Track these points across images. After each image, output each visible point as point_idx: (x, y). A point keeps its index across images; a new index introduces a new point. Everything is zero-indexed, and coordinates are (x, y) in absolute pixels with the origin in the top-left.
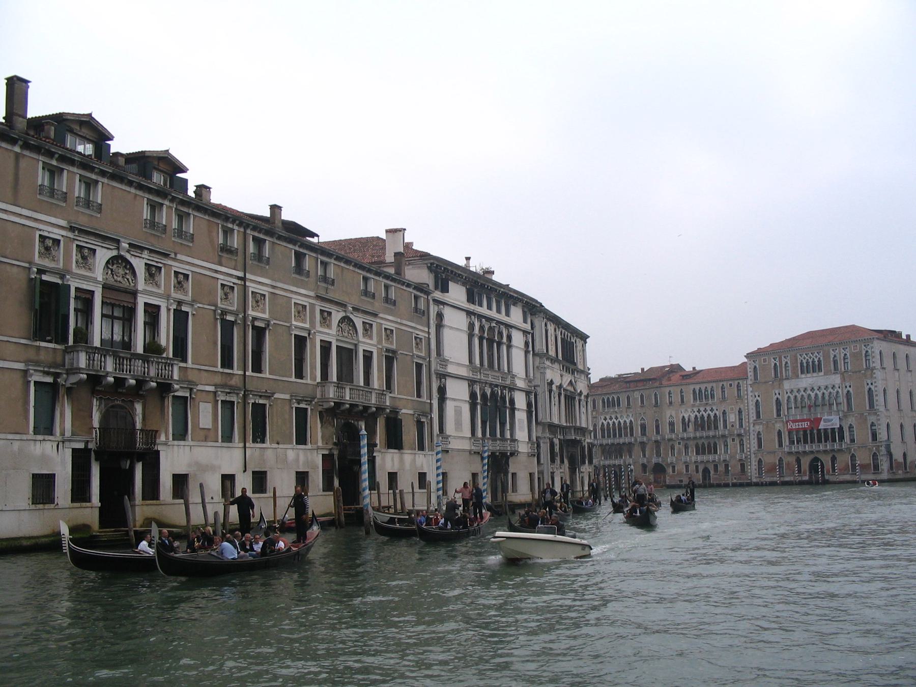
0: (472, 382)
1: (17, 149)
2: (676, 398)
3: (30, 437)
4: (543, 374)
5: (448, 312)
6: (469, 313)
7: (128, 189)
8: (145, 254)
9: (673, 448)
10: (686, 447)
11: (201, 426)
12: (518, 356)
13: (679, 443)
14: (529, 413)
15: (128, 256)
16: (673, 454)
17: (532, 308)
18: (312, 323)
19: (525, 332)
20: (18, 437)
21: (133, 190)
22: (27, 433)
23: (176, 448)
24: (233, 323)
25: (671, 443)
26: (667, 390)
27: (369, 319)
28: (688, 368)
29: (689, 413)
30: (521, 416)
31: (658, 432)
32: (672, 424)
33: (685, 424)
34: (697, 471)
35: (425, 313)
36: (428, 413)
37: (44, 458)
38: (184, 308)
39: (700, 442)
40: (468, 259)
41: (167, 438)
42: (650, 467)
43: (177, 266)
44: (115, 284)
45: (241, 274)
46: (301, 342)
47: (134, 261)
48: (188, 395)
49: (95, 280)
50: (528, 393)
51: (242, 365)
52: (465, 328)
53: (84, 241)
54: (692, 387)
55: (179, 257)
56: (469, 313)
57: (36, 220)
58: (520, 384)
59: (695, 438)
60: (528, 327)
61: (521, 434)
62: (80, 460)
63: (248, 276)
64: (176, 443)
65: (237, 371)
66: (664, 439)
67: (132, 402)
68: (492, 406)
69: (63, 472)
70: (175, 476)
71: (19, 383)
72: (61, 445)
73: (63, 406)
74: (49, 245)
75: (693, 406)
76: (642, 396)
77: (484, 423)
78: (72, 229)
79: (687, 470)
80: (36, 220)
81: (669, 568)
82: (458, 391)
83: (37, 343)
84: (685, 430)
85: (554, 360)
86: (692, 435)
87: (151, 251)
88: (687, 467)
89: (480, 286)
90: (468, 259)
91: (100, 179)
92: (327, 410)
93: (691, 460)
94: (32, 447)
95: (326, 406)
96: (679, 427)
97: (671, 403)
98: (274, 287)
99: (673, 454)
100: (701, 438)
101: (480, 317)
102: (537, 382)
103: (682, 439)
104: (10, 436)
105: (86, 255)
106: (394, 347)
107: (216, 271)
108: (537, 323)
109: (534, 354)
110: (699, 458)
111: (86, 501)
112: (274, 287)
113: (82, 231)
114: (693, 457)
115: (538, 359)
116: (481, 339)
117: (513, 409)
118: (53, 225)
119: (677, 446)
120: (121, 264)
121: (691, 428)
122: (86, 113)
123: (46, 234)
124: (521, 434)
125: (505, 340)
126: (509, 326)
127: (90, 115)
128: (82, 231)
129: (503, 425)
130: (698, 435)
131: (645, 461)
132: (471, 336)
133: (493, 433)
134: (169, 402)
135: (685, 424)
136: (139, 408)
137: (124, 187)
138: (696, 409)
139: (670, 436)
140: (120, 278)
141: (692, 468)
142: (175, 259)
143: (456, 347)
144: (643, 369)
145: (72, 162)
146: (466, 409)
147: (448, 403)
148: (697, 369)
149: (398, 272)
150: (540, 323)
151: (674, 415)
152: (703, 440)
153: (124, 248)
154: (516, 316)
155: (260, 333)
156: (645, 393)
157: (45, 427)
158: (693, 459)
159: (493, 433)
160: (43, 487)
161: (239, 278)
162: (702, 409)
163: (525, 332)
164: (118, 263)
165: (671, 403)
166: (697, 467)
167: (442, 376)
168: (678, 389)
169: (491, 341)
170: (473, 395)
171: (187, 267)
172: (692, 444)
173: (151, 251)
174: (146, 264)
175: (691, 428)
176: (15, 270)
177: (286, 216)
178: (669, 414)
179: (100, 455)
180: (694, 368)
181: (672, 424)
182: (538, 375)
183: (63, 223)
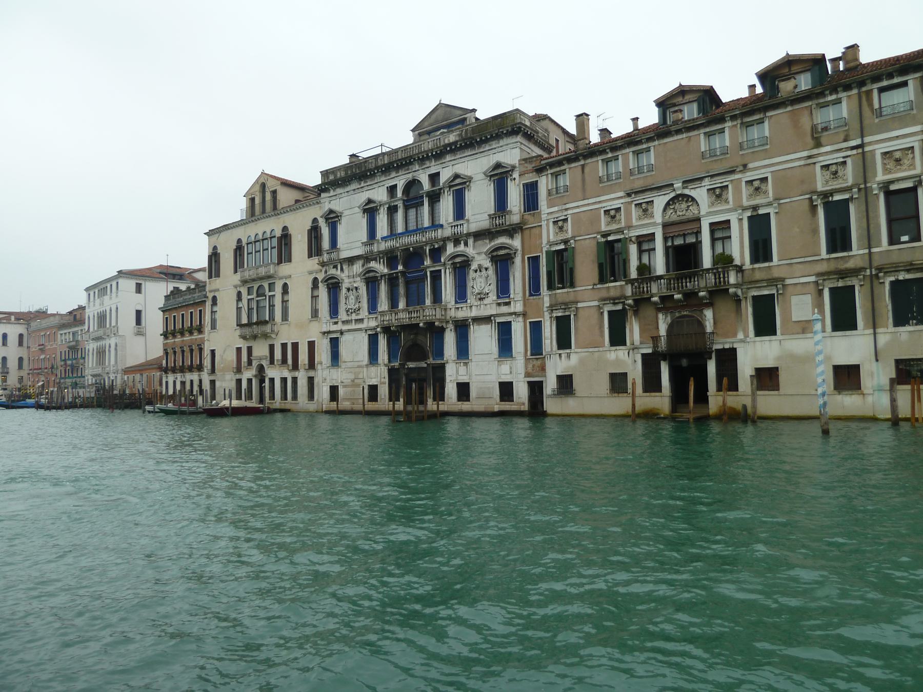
3: (605, 349)
7: (680, 137)
8: (707, 182)
11: (794, 319)
15: (687, 192)
20: (596, 349)
21: (684, 135)
22: (604, 346)
23: (758, 343)
37: (618, 361)
38: (761, 211)
40: (635, 120)
41: (746, 336)
43: (749, 176)
44: (678, 218)
45: (857, 142)
47: (693, 193)
48: (774, 292)
49: (655, 224)
51: (866, 242)
53: (640, 199)
55: (751, 166)
57: (600, 202)
62: (650, 364)
64: (758, 339)
65: (857, 250)
67: (701, 311)
69: (636, 373)
71: (596, 315)
72: (631, 352)
73: (631, 324)
74: (612, 214)
78: (629, 195)
80: (600, 202)
81: (729, 577)
83: (607, 285)
90: (635, 120)
91: (651, 144)
94: (608, 356)
104: (591, 350)
105: (646, 209)
113: (636, 193)
118: (614, 199)
120: (683, 200)
123: (609, 208)
127: (681, 85)
137: (676, 138)
140: (682, 211)
145: (621, 147)
153: (678, 188)
157: (618, 338)
160: (618, 382)
164: (679, 201)
171: (763, 171)
174: (708, 190)
176: (588, 241)
179: (671, 357)
183: (621, 194)
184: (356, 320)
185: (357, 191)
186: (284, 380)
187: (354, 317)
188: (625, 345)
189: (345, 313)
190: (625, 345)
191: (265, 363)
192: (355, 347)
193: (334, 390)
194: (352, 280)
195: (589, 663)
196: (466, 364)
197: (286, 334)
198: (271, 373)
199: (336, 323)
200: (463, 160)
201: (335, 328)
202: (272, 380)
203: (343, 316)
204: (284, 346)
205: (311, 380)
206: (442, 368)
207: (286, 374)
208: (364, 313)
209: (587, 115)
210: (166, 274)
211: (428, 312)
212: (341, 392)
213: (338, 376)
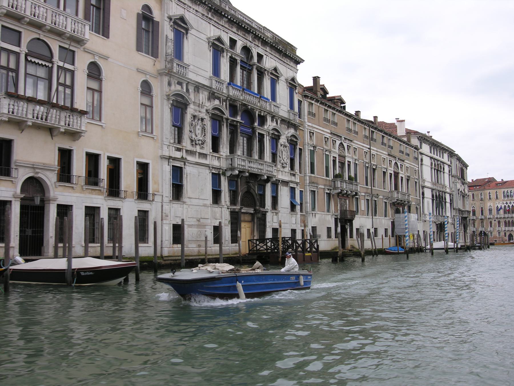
0: (432, 190)
1: (318, 104)
2: (493, 196)
4: (456, 185)
5: (424, 158)
6: (431, 158)
9: (491, 223)
10: (499, 222)
12: (446, 176)
13: (495, 220)
14: (451, 204)
16: (491, 226)
17: (451, 154)
18: (387, 166)
19: (449, 166)
21: (343, 116)
24: (368, 167)
25: (490, 220)
26: (488, 191)
27: (402, 163)
28: (499, 180)
29: (500, 204)
30: (448, 205)
31: (482, 214)
32: (490, 210)
33: (498, 210)
34: (505, 236)
35: (417, 159)
36: (419, 205)
39: (507, 220)
40: (428, 132)
42: (477, 233)
46: (384, 173)
50: (450, 194)
52: (429, 165)
54: (503, 190)
56: (431, 158)
58: (448, 190)
59: (504, 218)
60: (449, 163)
61: (448, 214)
63: (371, 148)
66: (486, 218)
68: (439, 200)
70: (312, 227)
75: (503, 200)
76: (473, 195)
77: (436, 208)
78: (331, 133)
79: (499, 235)
82: (428, 194)
84: (498, 213)
85: (459, 179)
86: (502, 216)
87: (349, 140)
88: (499, 233)
89: (435, 145)
91: (337, 113)
92: (394, 203)
93: (502, 230)
95: (393, 201)
96: (494, 212)
97: (490, 199)
98: (377, 151)
99: (491, 226)
100: (508, 218)
101: (435, 159)
102: (453, 189)
103: (497, 218)
106: (409, 175)
107: (363, 146)
108: (453, 161)
109: (452, 176)
110: (507, 229)
111: (145, 243)
112: (377, 151)
113: (334, 134)
114: (503, 228)
115: (453, 178)
116: (435, 169)
117: (445, 202)
119: (493, 222)
121: (502, 211)
122: (312, 80)
124: (448, 214)
125: (442, 170)
126: (444, 163)
128: (334, 134)
129: (442, 209)
130: (506, 216)
131: (475, 230)
132: (431, 168)
133: (439, 214)
134: (354, 199)
135: (498, 210)
136: (347, 201)
138: (505, 202)
139: (489, 217)
141: (502, 234)
142: (354, 143)
143: (427, 173)
144: (472, 180)
146: (431, 201)
147: (425, 199)
148: (505, 180)
149: (409, 140)
150: (454, 160)
151: (492, 205)
152: (509, 219)
154: (445, 158)
155: (374, 170)
156: (475, 193)
158: (503, 229)
159: (439, 214)
161: (369, 149)
162: (508, 202)
163: (449, 166)
165: (490, 199)
166: (505, 233)
167: (423, 187)
168: (495, 191)
169: (438, 171)
170: (433, 196)
172: (502, 221)
173: (349, 140)
175: (502, 211)
177: (379, 120)
178: (489, 204)
180: (502, 180)
181: (490, 210)
182: (454, 186)
183: (329, 131)
184: (200, 154)
185: (205, 18)
186: (92, 212)
187: (198, 149)
188: (59, 206)
189: (189, 142)
190: (59, 206)
191: (50, 178)
192: (198, 182)
193: (178, 232)
194: (197, 108)
195: (469, 341)
196: (277, 214)
197: (95, 140)
198: (59, 194)
199: (179, 150)
200: (277, 60)
201: (178, 155)
202: (64, 211)
203: (186, 144)
204: (93, 159)
205: (143, 217)
206: (264, 215)
207: (103, 203)
208: (208, 148)
209: (319, 78)
210: (221, 14)
211: (262, 167)
212: (188, 233)
213: (176, 212)
